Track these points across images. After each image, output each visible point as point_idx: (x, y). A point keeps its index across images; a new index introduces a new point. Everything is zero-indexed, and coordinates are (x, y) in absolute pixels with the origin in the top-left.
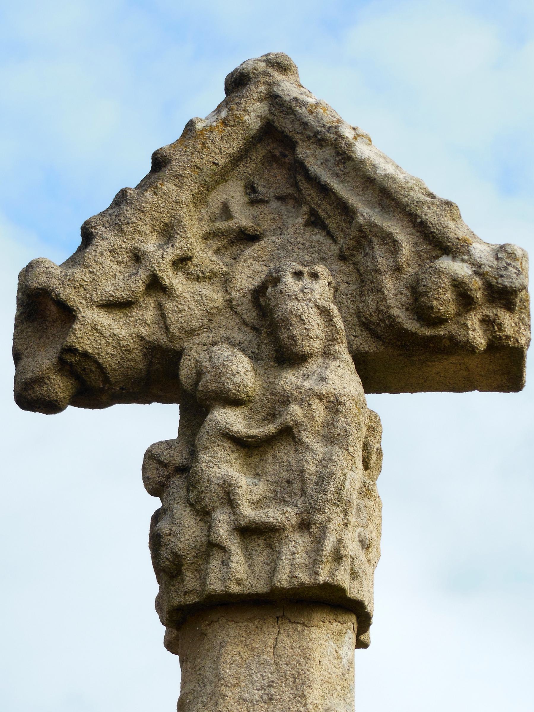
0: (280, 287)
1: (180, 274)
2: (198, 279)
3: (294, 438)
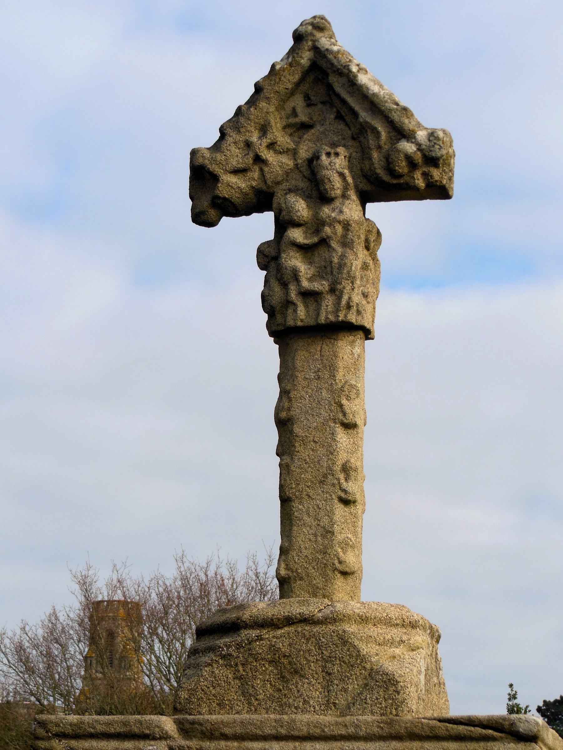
0: (319, 162)
1: (271, 151)
2: (280, 153)
3: (327, 244)
